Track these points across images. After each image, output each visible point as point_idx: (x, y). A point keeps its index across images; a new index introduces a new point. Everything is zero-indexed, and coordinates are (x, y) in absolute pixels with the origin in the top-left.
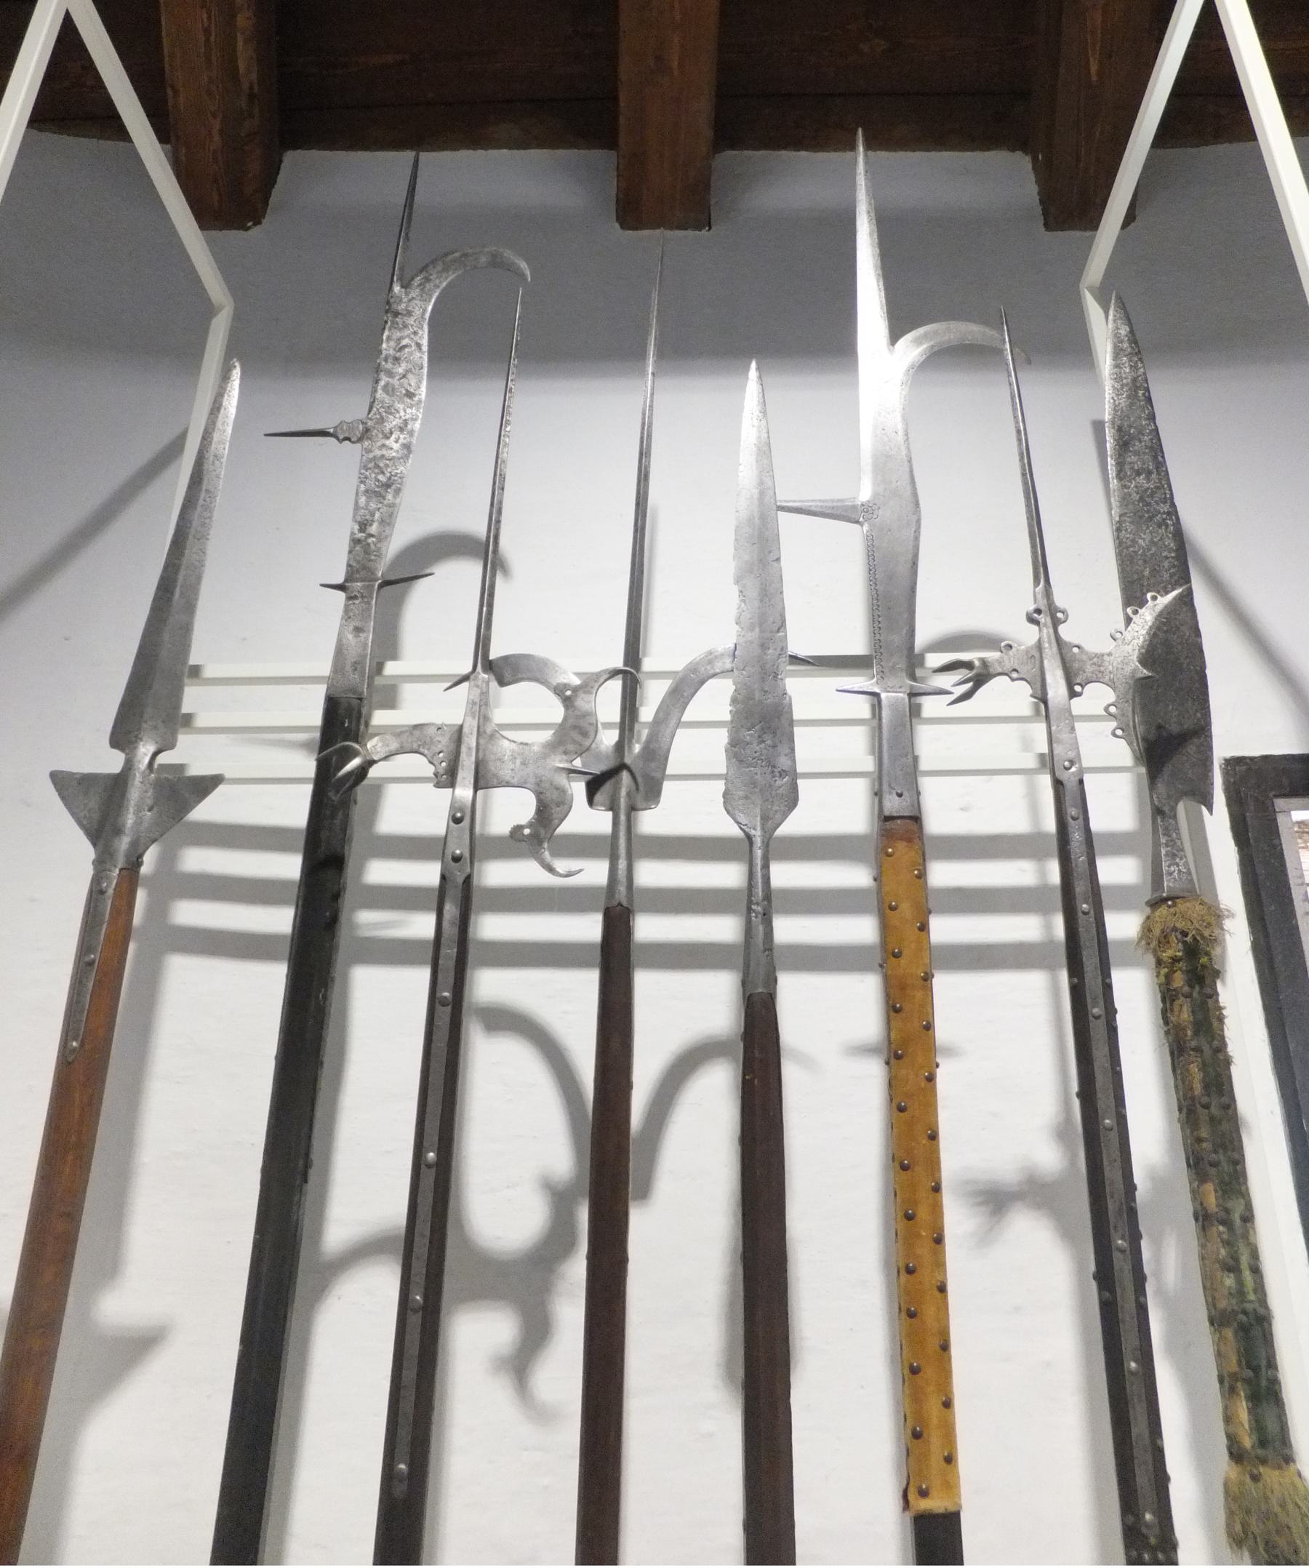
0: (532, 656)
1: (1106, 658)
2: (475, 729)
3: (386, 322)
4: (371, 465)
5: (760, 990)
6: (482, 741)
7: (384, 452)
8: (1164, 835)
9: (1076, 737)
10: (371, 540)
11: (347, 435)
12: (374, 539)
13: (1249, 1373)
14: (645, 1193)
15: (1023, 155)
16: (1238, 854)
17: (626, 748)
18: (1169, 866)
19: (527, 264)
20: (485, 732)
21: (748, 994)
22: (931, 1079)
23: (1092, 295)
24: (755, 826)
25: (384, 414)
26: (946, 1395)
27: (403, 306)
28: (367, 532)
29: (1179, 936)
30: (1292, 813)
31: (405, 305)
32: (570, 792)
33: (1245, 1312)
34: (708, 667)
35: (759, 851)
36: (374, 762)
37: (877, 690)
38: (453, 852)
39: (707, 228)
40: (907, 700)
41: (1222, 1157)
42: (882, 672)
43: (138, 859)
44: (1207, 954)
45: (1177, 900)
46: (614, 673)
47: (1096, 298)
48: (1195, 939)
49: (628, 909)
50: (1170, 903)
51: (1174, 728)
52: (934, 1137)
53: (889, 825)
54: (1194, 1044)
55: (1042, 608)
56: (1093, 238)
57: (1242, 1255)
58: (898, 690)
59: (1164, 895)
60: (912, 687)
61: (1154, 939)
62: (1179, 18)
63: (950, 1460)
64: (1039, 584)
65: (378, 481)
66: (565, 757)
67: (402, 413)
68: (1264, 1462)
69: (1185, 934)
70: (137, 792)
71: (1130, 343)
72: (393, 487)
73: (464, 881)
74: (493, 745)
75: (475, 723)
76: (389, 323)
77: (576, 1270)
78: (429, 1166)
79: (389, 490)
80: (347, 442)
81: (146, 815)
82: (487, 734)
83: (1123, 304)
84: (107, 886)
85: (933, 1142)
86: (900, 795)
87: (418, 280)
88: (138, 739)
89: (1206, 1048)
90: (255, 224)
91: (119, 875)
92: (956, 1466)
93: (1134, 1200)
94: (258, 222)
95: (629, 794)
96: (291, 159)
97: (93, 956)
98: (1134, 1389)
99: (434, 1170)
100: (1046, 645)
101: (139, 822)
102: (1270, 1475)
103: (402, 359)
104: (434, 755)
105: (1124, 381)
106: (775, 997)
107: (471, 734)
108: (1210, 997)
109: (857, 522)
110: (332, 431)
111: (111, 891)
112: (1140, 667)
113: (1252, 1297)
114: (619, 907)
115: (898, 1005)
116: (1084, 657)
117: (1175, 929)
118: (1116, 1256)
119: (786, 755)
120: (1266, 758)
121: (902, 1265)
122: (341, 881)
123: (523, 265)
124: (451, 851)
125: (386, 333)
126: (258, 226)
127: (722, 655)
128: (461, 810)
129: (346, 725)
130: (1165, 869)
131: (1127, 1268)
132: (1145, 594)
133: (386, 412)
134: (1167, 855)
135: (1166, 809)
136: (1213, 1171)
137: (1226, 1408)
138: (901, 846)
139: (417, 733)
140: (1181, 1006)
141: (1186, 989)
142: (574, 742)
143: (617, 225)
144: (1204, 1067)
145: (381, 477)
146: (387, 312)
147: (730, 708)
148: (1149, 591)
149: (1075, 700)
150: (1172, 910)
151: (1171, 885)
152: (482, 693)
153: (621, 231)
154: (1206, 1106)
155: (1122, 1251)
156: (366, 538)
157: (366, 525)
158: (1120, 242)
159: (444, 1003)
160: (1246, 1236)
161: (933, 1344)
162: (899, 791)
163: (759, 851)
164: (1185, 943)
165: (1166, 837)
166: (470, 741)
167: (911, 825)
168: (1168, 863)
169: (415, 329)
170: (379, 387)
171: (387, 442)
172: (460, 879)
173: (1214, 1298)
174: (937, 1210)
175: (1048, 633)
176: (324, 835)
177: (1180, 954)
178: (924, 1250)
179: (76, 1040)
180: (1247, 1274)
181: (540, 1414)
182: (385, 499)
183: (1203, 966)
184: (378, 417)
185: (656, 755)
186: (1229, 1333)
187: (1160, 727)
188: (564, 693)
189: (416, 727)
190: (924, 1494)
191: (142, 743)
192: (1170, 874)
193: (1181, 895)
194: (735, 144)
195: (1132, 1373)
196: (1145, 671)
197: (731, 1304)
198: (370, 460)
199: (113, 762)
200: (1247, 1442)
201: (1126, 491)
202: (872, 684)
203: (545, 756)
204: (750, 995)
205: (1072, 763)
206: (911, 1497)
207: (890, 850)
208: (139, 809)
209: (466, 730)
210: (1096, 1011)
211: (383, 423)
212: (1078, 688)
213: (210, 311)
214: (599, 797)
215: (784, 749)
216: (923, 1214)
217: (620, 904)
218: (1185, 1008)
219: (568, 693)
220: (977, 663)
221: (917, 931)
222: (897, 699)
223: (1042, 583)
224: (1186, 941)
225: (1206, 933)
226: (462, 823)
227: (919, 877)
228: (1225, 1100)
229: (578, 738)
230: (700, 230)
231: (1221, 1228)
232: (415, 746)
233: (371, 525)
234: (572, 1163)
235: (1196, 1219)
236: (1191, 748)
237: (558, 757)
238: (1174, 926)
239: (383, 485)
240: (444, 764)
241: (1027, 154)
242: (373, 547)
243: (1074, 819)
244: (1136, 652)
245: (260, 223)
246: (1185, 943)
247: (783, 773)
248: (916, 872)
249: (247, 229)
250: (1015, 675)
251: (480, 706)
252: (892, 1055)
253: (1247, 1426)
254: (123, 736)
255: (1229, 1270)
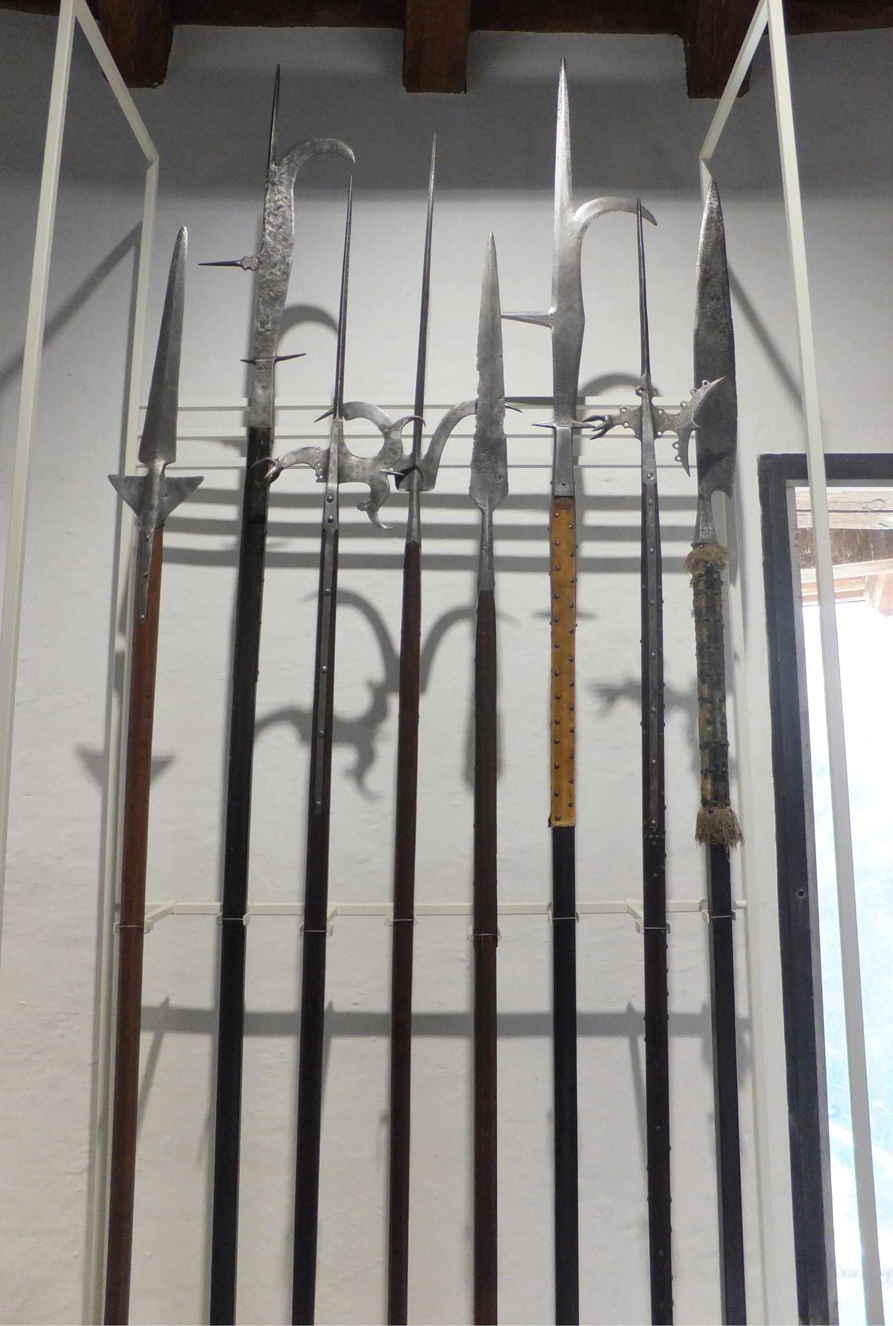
0: (364, 403)
1: (676, 417)
2: (337, 450)
3: (267, 190)
4: (265, 286)
5: (486, 589)
6: (340, 457)
7: (272, 277)
8: (703, 510)
9: (655, 461)
10: (268, 333)
11: (249, 266)
12: (270, 333)
13: (714, 769)
14: (424, 688)
15: (679, 38)
16: (762, 511)
17: (417, 458)
18: (704, 527)
19: (353, 151)
20: (342, 452)
21: (480, 590)
22: (572, 632)
23: (706, 165)
24: (486, 504)
25: (270, 252)
26: (571, 778)
27: (277, 179)
28: (265, 328)
29: (704, 563)
30: (796, 488)
31: (278, 178)
32: (388, 484)
33: (715, 742)
34: (462, 412)
35: (487, 518)
36: (283, 468)
37: (555, 426)
38: (329, 518)
39: (463, 92)
40: (570, 431)
41: (713, 672)
42: (558, 415)
43: (163, 522)
44: (718, 573)
45: (705, 545)
46: (410, 419)
47: (707, 167)
48: (712, 565)
49: (418, 544)
50: (701, 546)
51: (715, 451)
52: (572, 660)
53: (558, 501)
54: (706, 618)
55: (644, 388)
56: (717, 104)
57: (717, 717)
58: (566, 425)
59: (699, 542)
60: (573, 424)
61: (692, 564)
62: (755, 24)
63: (571, 805)
64: (644, 373)
65: (270, 295)
66: (385, 465)
67: (281, 252)
68: (715, 805)
69: (707, 562)
70: (157, 486)
71: (717, 214)
72: (279, 300)
73: (335, 533)
74: (347, 459)
75: (337, 447)
76: (269, 190)
77: (391, 726)
78: (323, 672)
79: (277, 302)
80: (249, 270)
81: (164, 499)
82: (343, 453)
83: (717, 188)
84: (150, 537)
85: (572, 663)
86: (564, 485)
87: (285, 160)
88: (154, 457)
89: (711, 619)
90: (160, 84)
91: (155, 531)
92: (574, 809)
93: (663, 690)
94: (161, 83)
95: (418, 483)
96: (179, 31)
97: (146, 573)
98: (654, 771)
99: (326, 675)
100: (644, 409)
101: (161, 502)
102: (717, 811)
103: (279, 215)
104: (315, 464)
105: (711, 239)
106: (494, 592)
107: (335, 453)
108: (717, 594)
109: (548, 326)
110: (239, 263)
111: (151, 540)
112: (694, 423)
113: (720, 735)
114: (413, 544)
115: (557, 595)
116: (665, 416)
117: (702, 560)
118: (652, 715)
119: (502, 467)
120: (784, 456)
121: (553, 720)
122: (265, 530)
123: (351, 152)
124: (328, 516)
125: (268, 197)
126: (162, 85)
127: (469, 405)
128: (332, 495)
129: (262, 443)
130: (701, 529)
131: (656, 720)
132: (702, 381)
133: (271, 251)
134: (703, 521)
135: (706, 496)
136: (708, 678)
137: (703, 784)
138: (564, 511)
139: (305, 452)
140: (701, 598)
141: (705, 590)
142: (390, 457)
143: (404, 89)
144: (709, 629)
145: (272, 293)
146: (267, 182)
147: (474, 441)
148: (703, 379)
149: (657, 440)
150: (702, 549)
151: (703, 536)
152: (340, 430)
153: (406, 93)
154: (709, 648)
155: (654, 712)
156: (265, 332)
157: (264, 324)
158: (735, 105)
159: (327, 594)
160: (721, 709)
161: (567, 755)
162: (564, 483)
163: (487, 518)
164: (706, 567)
165: (703, 511)
166: (334, 457)
167: (569, 501)
168: (703, 525)
169: (286, 195)
170: (266, 234)
171: (274, 271)
172: (333, 531)
173: (702, 736)
174: (572, 695)
175: (646, 402)
176: (254, 505)
177: (703, 573)
178: (564, 713)
179: (144, 615)
180: (719, 725)
181: (371, 797)
182: (274, 308)
183: (715, 580)
184: (267, 254)
185: (433, 460)
186: (707, 751)
187: (707, 450)
188: (384, 430)
189: (304, 449)
190: (558, 819)
191: (157, 459)
192: (703, 531)
193: (708, 542)
194: (485, 26)
195: (653, 764)
196: (696, 425)
197: (469, 745)
198: (264, 283)
199: (142, 472)
200: (709, 798)
201: (704, 310)
202: (552, 422)
203: (374, 465)
204: (481, 591)
205: (652, 475)
206: (552, 821)
207: (557, 514)
208: (160, 496)
209: (332, 451)
210: (652, 602)
211: (270, 258)
212: (659, 433)
213: (145, 164)
214: (401, 484)
215: (500, 464)
216: (565, 696)
217: (414, 542)
218: (703, 600)
219: (386, 430)
220: (607, 418)
221: (569, 557)
222: (565, 430)
223: (646, 372)
224: (707, 566)
225: (718, 562)
226: (333, 502)
227: (572, 528)
228: (718, 645)
229: (392, 455)
230: (459, 93)
231: (709, 705)
232: (305, 459)
233: (267, 324)
234: (384, 674)
235: (699, 701)
236: (724, 462)
237: (382, 466)
238: (702, 558)
239: (273, 298)
240: (320, 470)
241: (681, 37)
242: (269, 337)
243: (650, 505)
244: (693, 414)
245: (162, 83)
246: (706, 567)
247: (500, 477)
248: (570, 526)
249: (154, 87)
250: (626, 424)
251: (339, 437)
252: (553, 621)
253: (710, 791)
254: (146, 455)
255: (711, 724)
